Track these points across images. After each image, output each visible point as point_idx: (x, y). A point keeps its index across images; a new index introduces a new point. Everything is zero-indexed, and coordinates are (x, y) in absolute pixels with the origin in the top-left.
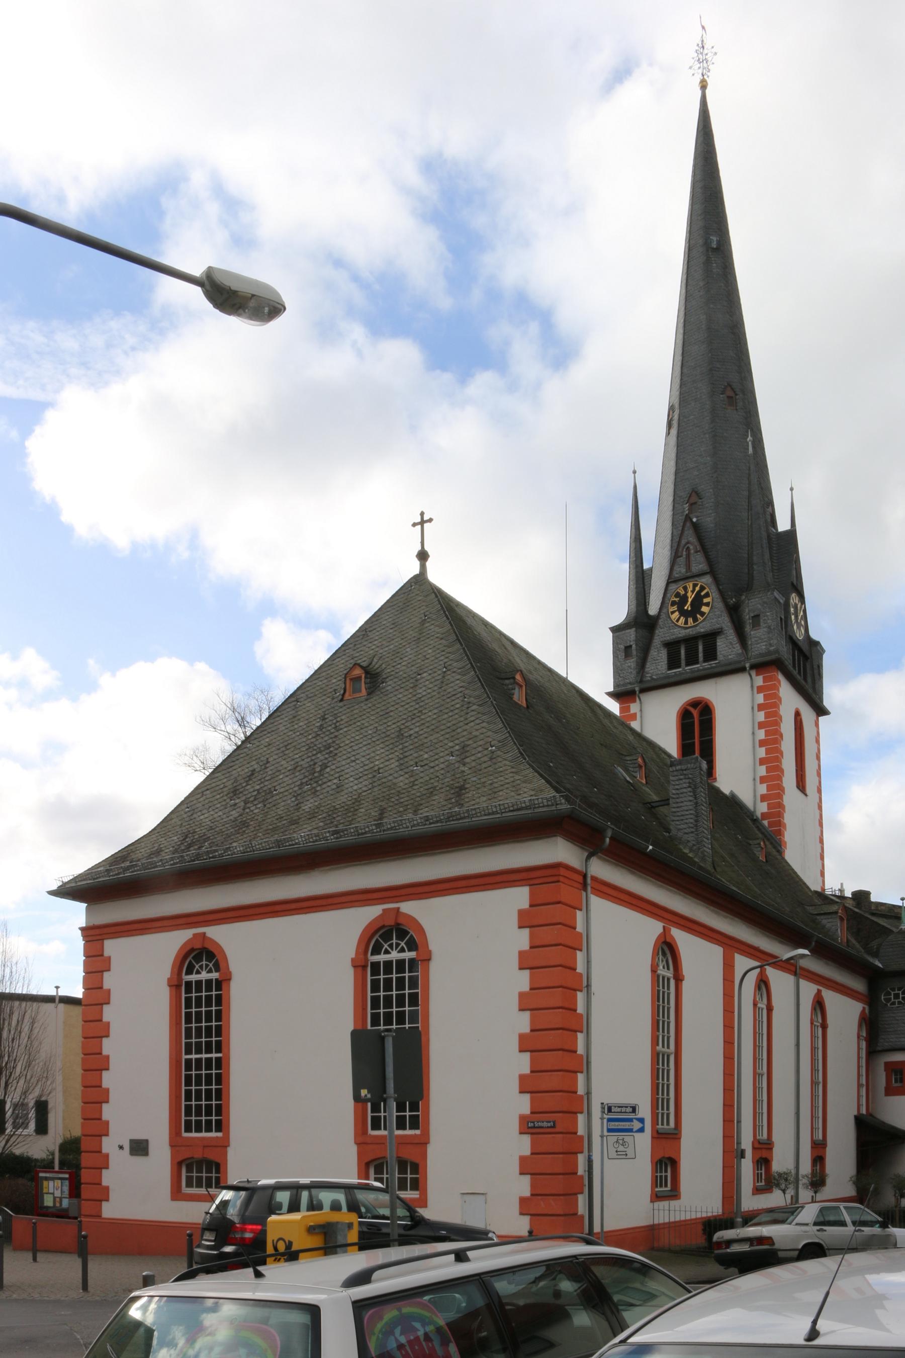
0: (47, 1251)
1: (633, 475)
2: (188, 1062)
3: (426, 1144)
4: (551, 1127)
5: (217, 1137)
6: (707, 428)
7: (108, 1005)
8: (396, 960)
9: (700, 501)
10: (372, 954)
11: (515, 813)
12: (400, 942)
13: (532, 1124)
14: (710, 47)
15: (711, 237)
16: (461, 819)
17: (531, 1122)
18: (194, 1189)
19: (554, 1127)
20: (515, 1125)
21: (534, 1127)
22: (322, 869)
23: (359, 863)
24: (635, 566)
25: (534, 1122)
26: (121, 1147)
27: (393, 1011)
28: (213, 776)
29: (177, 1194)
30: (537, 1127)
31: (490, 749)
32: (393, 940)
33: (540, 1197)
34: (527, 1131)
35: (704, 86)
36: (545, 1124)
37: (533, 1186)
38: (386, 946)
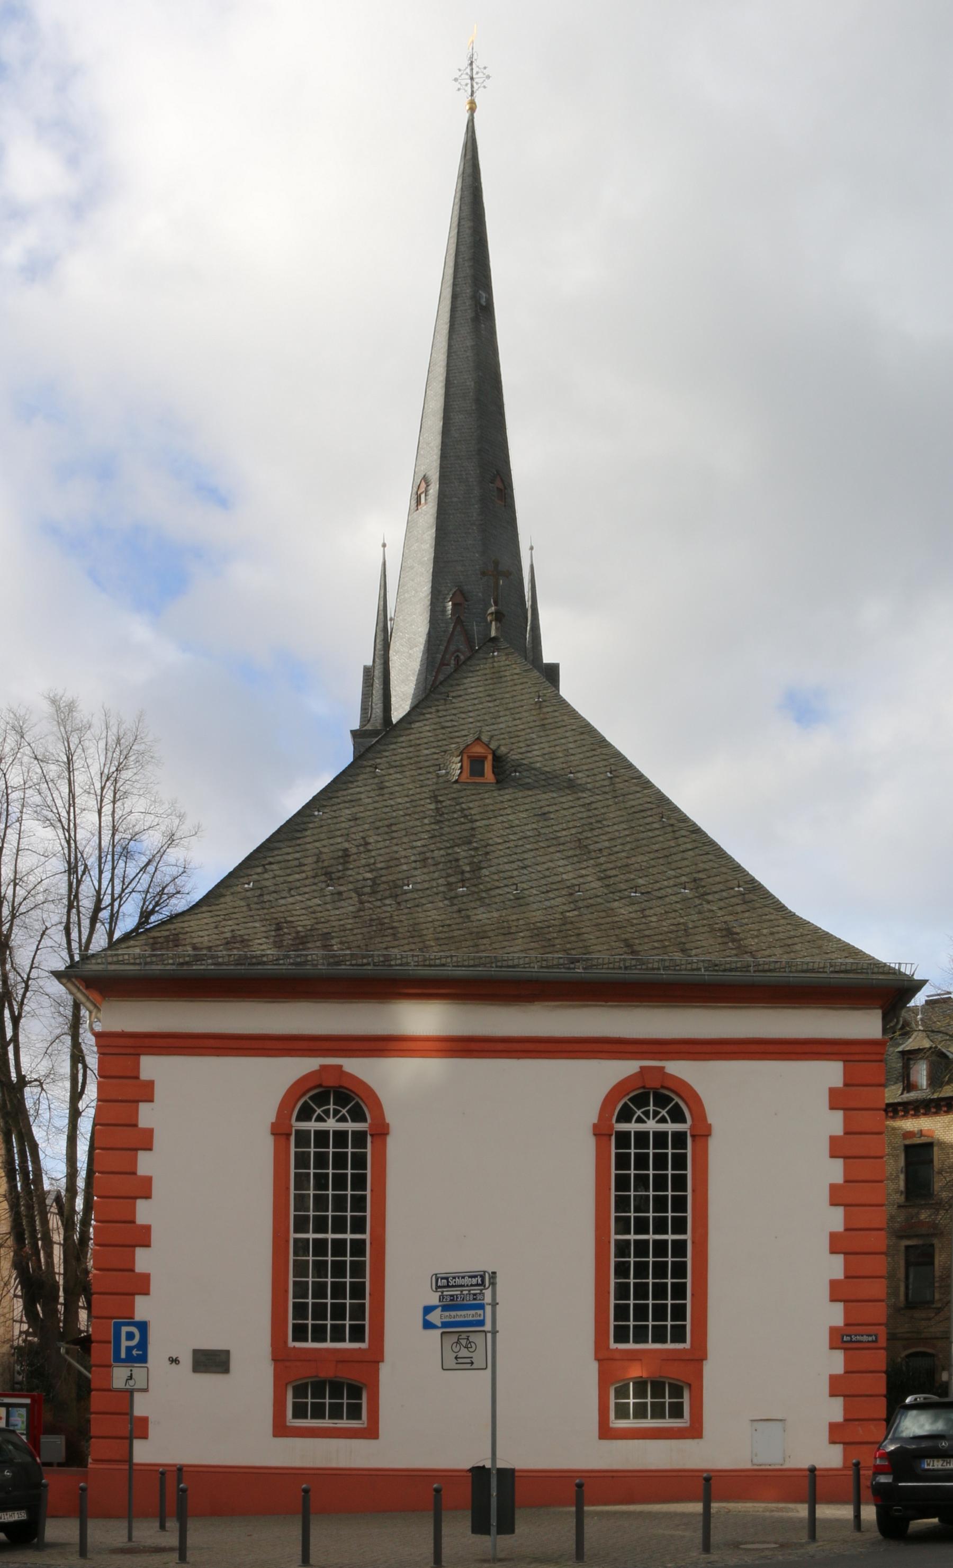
0: (53, 1517)
1: (382, 549)
2: (301, 1247)
3: (702, 1360)
4: (873, 1341)
5: (360, 1349)
6: (474, 518)
7: (148, 1152)
8: (672, 1132)
9: (467, 603)
10: (618, 1121)
11: (842, 975)
12: (660, 1110)
13: (849, 1338)
14: (482, 67)
15: (481, 292)
16: (770, 971)
17: (847, 1336)
18: (309, 1420)
19: (876, 1341)
20: (824, 1338)
21: (851, 1341)
22: (547, 1003)
23: (604, 1003)
24: (382, 661)
25: (850, 1336)
26: (174, 1361)
27: (347, 1195)
28: (271, 846)
29: (280, 1429)
30: (854, 1342)
31: (737, 889)
32: (649, 1105)
33: (857, 1423)
34: (842, 1345)
35: (472, 109)
36: (865, 1338)
37: (846, 1409)
38: (639, 1113)
